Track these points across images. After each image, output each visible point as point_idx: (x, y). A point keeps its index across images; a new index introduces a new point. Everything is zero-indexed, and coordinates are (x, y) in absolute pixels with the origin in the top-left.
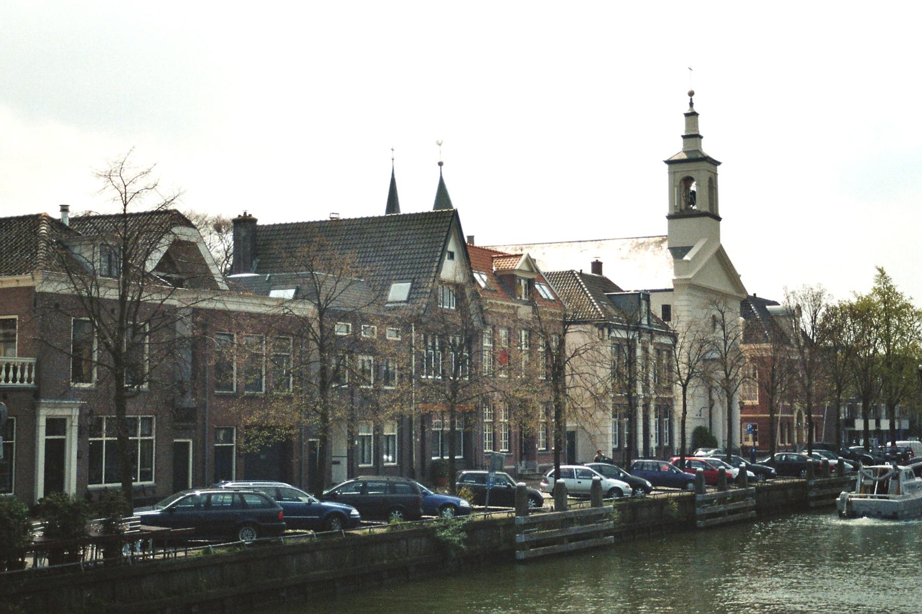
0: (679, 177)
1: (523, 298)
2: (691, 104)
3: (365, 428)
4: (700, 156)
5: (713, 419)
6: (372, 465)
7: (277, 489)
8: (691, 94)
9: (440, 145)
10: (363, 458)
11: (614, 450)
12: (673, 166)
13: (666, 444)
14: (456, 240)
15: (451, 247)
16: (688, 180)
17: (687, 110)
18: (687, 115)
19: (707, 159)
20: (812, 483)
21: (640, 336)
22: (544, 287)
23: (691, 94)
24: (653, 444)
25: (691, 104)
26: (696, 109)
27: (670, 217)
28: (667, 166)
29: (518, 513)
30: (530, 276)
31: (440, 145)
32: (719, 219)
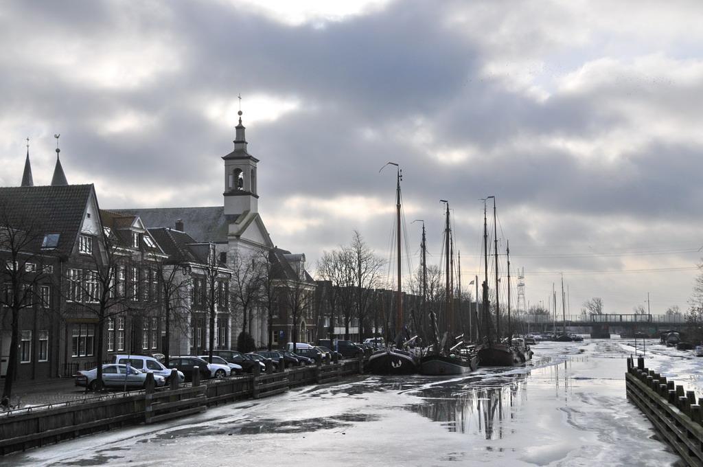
0: (232, 168)
1: (135, 246)
2: (240, 121)
3: (43, 335)
4: (246, 155)
5: (252, 327)
6: (47, 360)
8: (240, 113)
9: (57, 137)
10: (41, 356)
11: (191, 349)
12: (227, 161)
13: (223, 344)
14: (92, 204)
15: (89, 210)
16: (237, 171)
19: (250, 157)
20: (320, 368)
22: (149, 239)
23: (240, 113)
24: (216, 344)
25: (240, 121)
27: (225, 194)
28: (224, 161)
29: (147, 393)
30: (141, 232)
31: (57, 137)
32: (257, 197)
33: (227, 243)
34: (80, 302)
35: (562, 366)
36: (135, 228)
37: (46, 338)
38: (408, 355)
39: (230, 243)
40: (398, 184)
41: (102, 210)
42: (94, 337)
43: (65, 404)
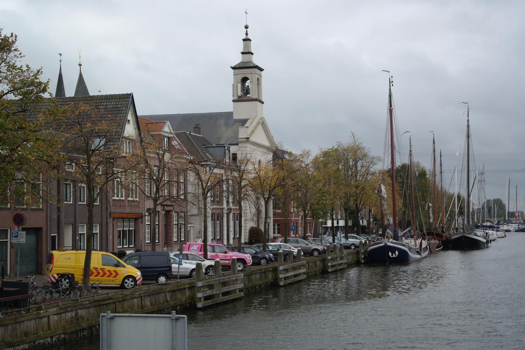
0: (240, 77)
2: (247, 34)
4: (252, 65)
7: (280, 245)
8: (246, 27)
13: (238, 236)
16: (245, 80)
17: (244, 37)
18: (244, 40)
21: (225, 172)
23: (246, 27)
25: (247, 34)
26: (249, 37)
33: (237, 144)
34: (138, 199)
35: (335, 225)
36: (165, 132)
37: (83, 231)
38: (404, 245)
39: (240, 145)
40: (390, 90)
41: (144, 118)
42: (134, 230)
43: (9, 273)
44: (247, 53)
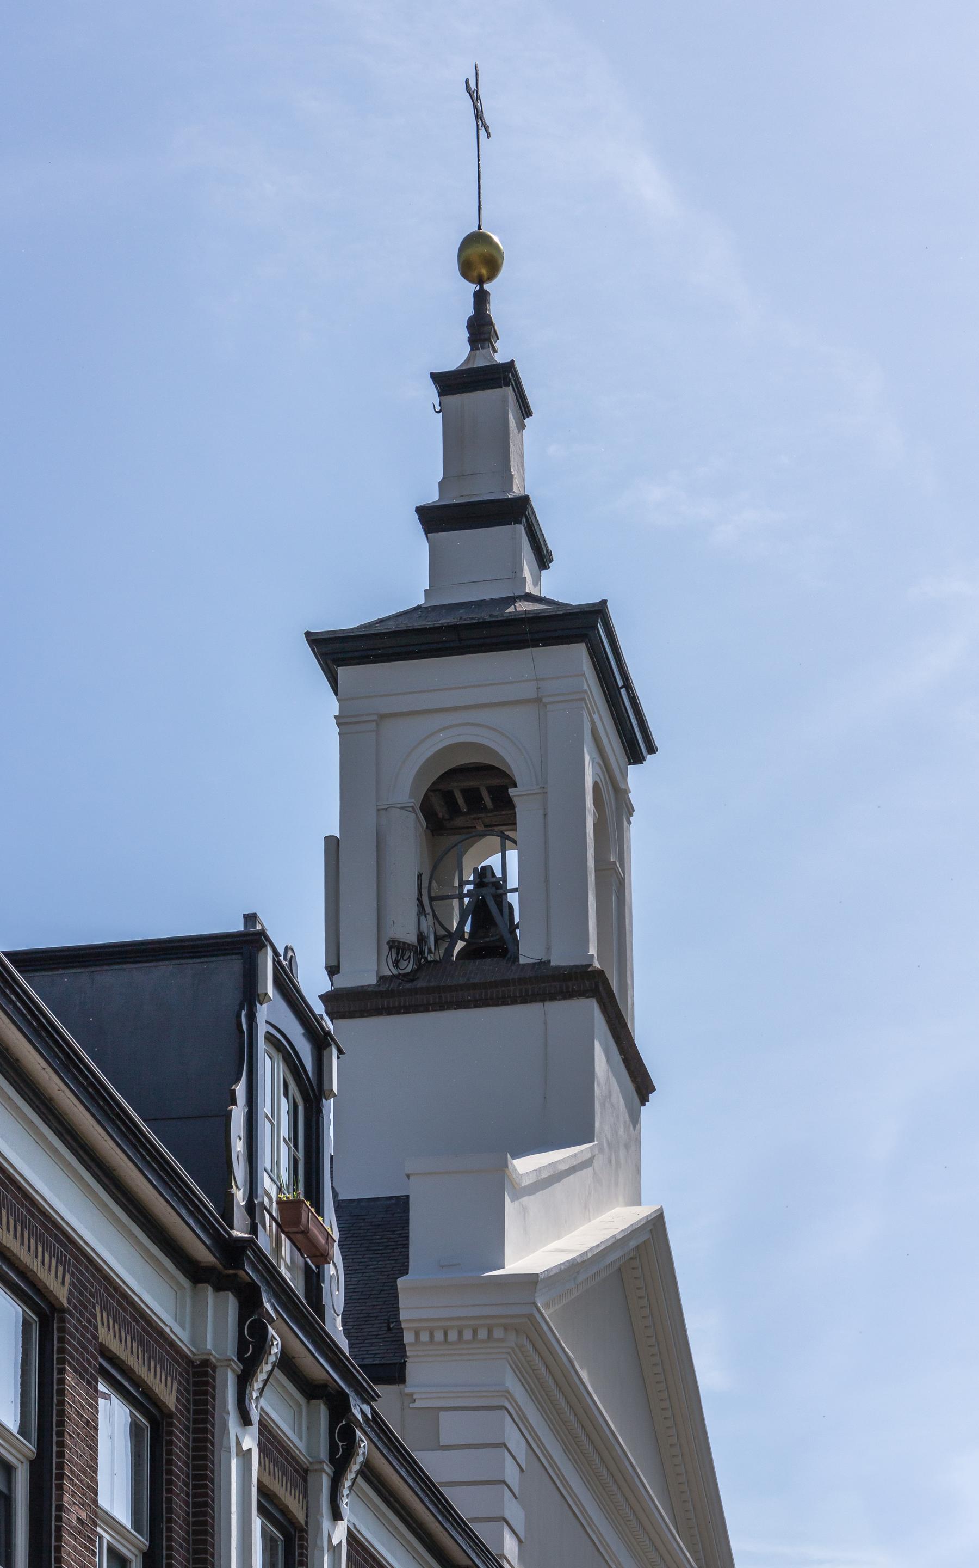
2: (481, 329)
8: (479, 259)
17: (455, 353)
18: (448, 384)
25: (481, 329)
44: (477, 511)
